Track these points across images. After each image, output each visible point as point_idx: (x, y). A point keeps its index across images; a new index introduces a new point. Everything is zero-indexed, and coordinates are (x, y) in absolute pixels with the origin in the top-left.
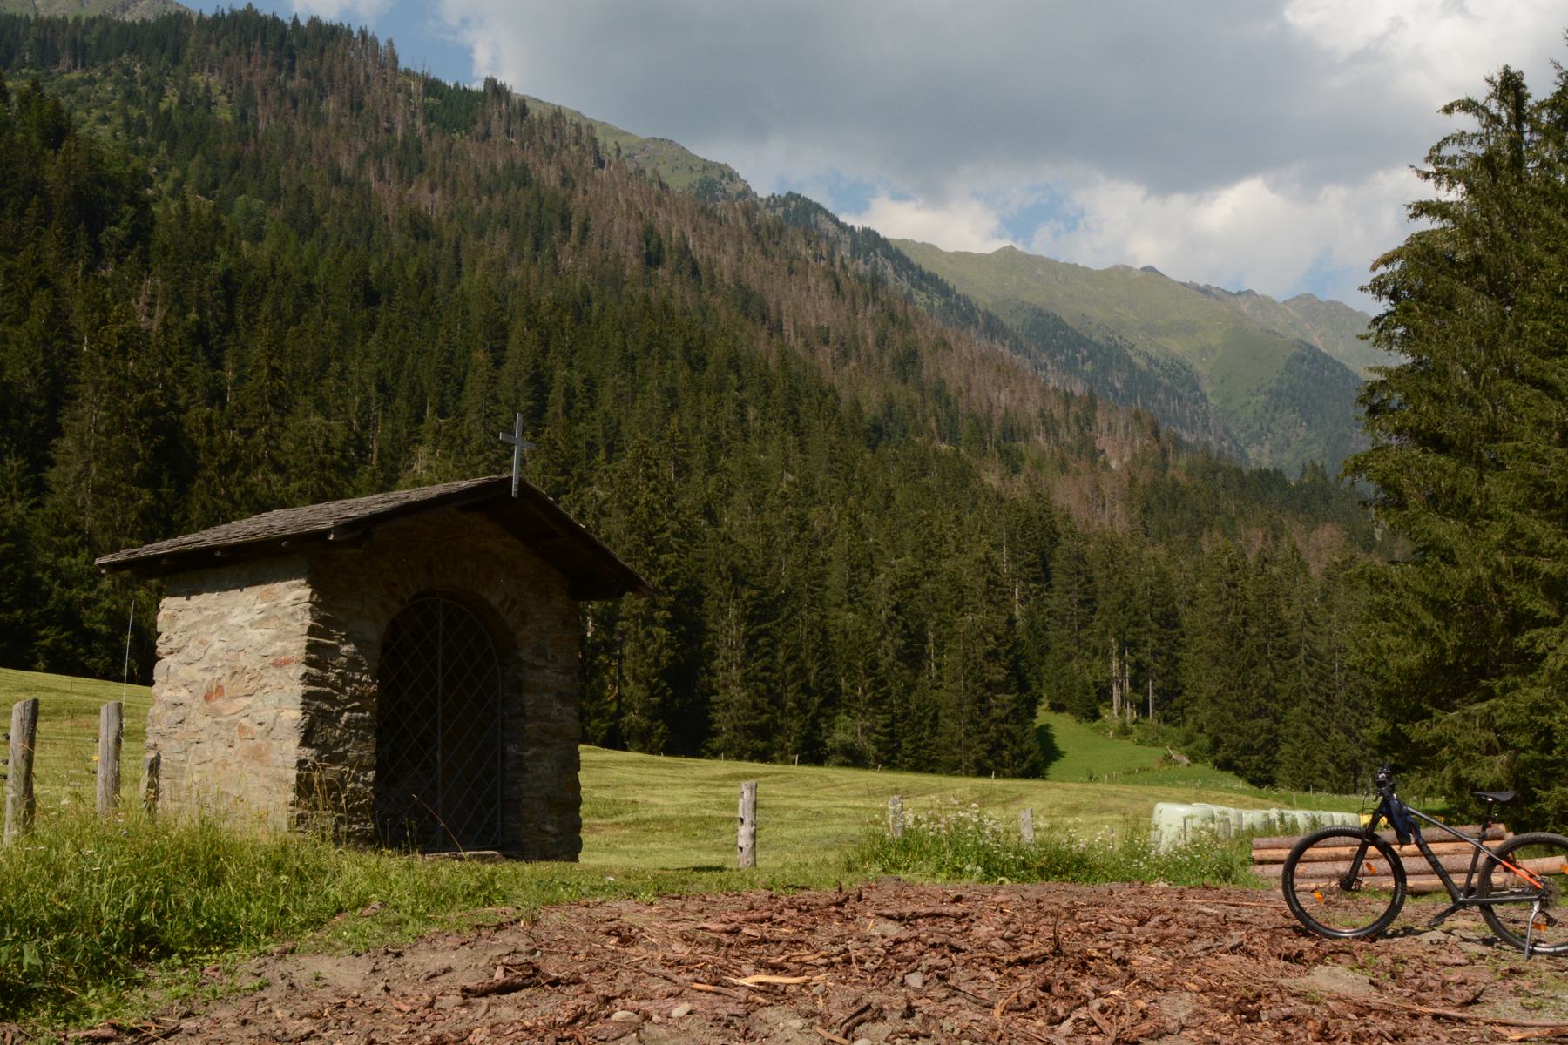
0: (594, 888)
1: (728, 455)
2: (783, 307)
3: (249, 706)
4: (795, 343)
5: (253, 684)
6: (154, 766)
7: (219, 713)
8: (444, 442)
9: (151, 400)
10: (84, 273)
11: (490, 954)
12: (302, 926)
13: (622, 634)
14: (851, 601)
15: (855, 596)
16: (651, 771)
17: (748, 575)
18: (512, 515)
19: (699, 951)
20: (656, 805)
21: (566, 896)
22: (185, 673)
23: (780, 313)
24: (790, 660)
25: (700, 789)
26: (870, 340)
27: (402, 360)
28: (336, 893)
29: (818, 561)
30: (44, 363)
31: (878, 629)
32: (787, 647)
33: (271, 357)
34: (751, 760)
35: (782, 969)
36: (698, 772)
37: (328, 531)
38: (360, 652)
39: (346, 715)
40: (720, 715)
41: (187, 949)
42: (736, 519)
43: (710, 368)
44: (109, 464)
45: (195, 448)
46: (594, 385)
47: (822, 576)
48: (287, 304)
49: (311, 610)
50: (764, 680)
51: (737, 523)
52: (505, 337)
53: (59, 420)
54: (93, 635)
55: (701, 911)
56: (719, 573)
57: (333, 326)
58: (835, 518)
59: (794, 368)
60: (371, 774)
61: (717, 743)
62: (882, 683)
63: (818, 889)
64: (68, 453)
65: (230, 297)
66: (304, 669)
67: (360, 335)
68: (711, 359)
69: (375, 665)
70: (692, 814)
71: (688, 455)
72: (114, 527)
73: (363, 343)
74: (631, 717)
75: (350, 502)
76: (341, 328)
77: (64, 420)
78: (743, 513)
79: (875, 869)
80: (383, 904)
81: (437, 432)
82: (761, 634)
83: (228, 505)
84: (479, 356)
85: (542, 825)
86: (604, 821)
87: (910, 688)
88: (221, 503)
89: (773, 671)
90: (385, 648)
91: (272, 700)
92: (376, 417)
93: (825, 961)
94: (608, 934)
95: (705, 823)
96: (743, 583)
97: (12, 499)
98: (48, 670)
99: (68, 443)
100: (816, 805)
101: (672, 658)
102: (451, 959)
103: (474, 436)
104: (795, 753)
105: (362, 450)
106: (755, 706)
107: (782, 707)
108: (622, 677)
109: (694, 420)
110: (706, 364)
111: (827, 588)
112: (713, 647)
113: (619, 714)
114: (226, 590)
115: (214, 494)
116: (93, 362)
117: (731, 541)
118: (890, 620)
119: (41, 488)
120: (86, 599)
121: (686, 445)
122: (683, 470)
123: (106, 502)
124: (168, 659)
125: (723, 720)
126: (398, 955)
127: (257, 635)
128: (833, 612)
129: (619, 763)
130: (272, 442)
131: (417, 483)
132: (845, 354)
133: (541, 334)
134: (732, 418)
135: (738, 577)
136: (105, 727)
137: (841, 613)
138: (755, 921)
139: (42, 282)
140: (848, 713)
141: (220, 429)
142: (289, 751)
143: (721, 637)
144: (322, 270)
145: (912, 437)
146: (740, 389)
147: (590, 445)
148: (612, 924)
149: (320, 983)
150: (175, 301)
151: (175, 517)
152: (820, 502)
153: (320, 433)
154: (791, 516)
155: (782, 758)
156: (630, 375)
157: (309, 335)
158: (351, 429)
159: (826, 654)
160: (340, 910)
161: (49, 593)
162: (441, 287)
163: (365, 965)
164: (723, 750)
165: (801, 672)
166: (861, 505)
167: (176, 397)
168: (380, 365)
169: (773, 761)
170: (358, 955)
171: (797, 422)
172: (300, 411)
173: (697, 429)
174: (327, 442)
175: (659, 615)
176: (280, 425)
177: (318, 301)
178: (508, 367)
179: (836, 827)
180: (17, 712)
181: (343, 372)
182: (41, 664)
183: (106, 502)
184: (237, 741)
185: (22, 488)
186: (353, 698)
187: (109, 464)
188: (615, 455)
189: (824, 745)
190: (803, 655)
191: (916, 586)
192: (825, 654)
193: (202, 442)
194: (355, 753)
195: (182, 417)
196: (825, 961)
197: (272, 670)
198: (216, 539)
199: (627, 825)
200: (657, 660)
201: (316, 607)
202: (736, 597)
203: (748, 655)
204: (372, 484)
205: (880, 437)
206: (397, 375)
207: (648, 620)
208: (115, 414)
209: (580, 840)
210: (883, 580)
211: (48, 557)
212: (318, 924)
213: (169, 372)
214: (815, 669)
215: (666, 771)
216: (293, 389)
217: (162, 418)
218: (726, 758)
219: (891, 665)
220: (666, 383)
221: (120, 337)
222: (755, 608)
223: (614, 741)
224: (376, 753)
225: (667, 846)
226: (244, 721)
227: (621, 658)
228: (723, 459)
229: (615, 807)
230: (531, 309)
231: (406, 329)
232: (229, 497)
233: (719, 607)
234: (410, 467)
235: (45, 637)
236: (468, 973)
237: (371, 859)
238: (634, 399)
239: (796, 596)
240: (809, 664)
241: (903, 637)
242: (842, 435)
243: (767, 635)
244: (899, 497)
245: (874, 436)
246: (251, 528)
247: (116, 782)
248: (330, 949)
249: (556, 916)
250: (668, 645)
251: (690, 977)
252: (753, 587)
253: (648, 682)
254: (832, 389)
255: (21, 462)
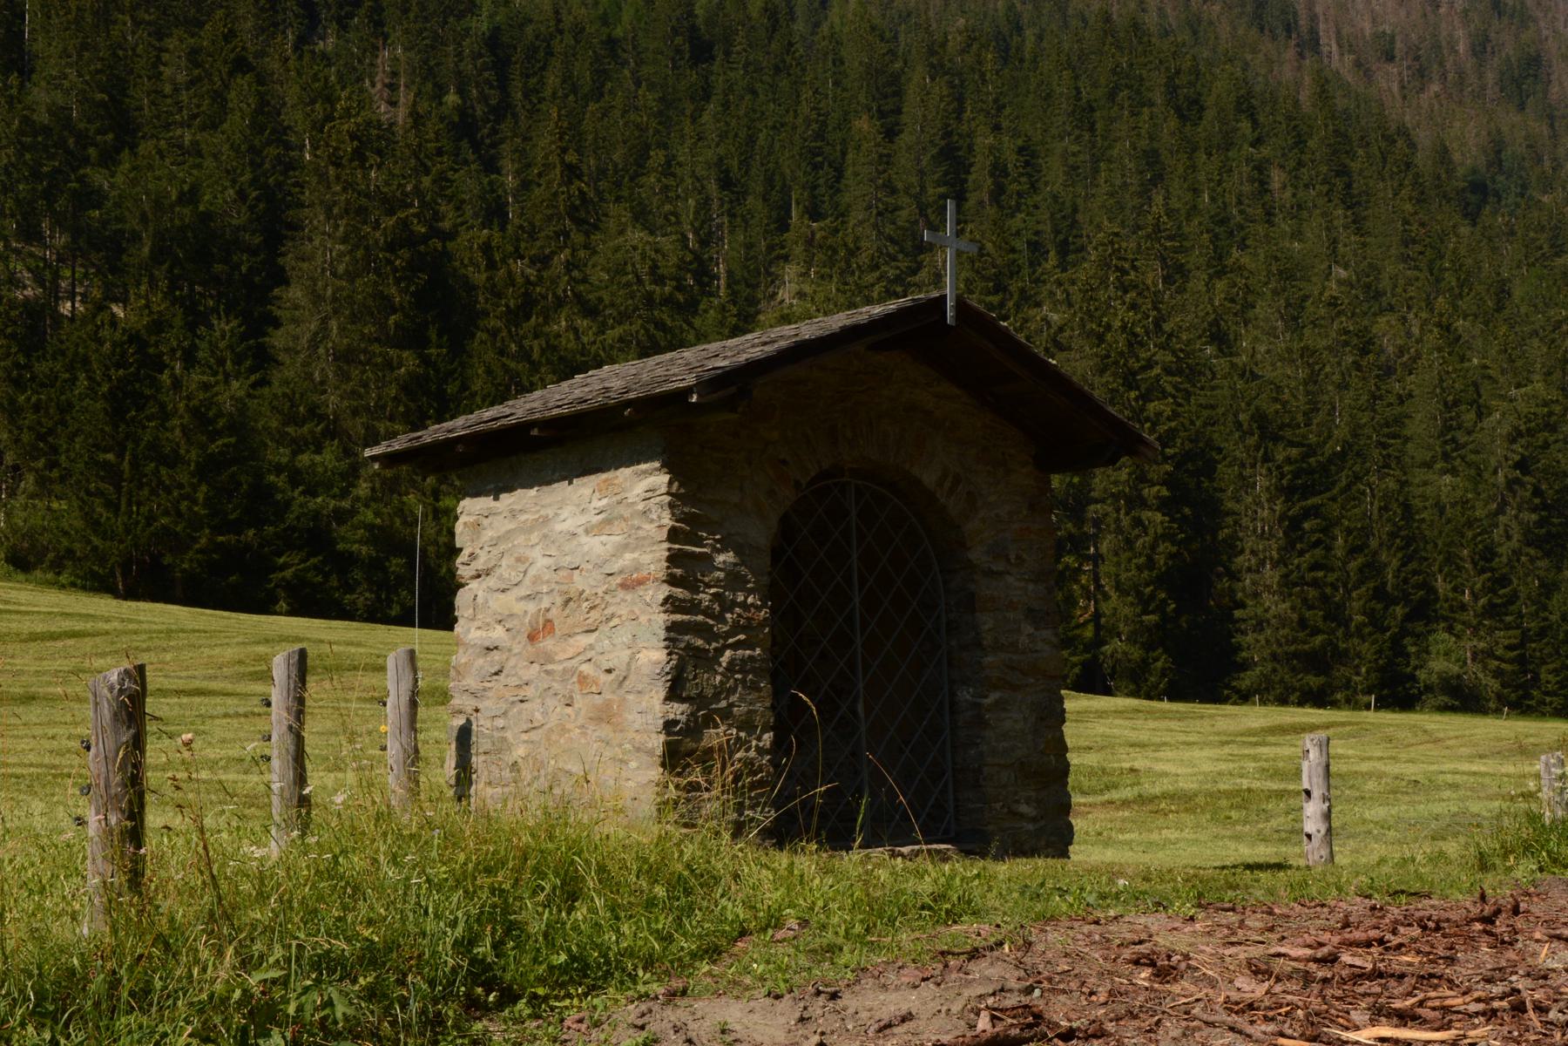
0: (1103, 896)
1: (1243, 246)
2: (1319, 9)
3: (591, 647)
4: (1340, 63)
5: (594, 614)
6: (464, 737)
7: (549, 659)
8: (820, 257)
9: (405, 223)
10: (296, 48)
11: (966, 993)
12: (694, 956)
13: (1097, 523)
14: (1446, 456)
15: (1452, 447)
16: (1152, 724)
17: (1282, 427)
18: (957, 351)
19: (1278, 988)
20: (1165, 774)
21: (1064, 908)
22: (499, 603)
23: (1314, 18)
24: (1353, 551)
25: (1227, 750)
26: (1461, 48)
27: (751, 140)
28: (735, 910)
29: (1392, 399)
30: (254, 181)
31: (1492, 498)
32: (1349, 531)
33: (564, 150)
34: (1301, 704)
35: (1415, 1018)
36: (1222, 724)
37: (688, 391)
38: (743, 563)
39: (728, 653)
40: (1250, 638)
41: (541, 991)
42: (1262, 343)
43: (1210, 114)
44: (354, 319)
45: (471, 288)
46: (1034, 155)
47: (1399, 421)
48: (583, 71)
49: (671, 506)
50: (1315, 583)
51: (1263, 349)
52: (898, 94)
53: (281, 261)
54: (345, 562)
55: (1271, 929)
56: (1239, 425)
57: (650, 98)
58: (1416, 331)
59: (1341, 103)
60: (768, 737)
61: (1247, 680)
62: (1503, 581)
63: (1445, 898)
64: (296, 307)
65: (501, 66)
66: (665, 590)
67: (689, 108)
68: (1209, 101)
69: (765, 580)
70: (1222, 787)
71: (1181, 250)
72: (367, 409)
73: (694, 120)
74: (1115, 646)
75: (714, 346)
76: (662, 100)
77: (288, 261)
78: (1272, 333)
79: (1524, 869)
80: (804, 923)
81: (810, 242)
82: (1307, 513)
83: (521, 367)
84: (863, 124)
85: (1028, 810)
86: (1090, 799)
87: (1548, 589)
88: (513, 365)
89: (1329, 569)
90: (776, 554)
91: (623, 636)
92: (720, 227)
93: (1481, 1006)
94: (1136, 963)
95: (1243, 799)
96: (1276, 439)
97: (227, 376)
98: (292, 612)
99: (296, 293)
100: (1410, 770)
101: (1172, 556)
102: (909, 1001)
103: (864, 244)
104: (1369, 693)
105: (704, 274)
106: (1302, 623)
107: (1346, 623)
108: (1099, 587)
109: (1189, 196)
110: (1202, 109)
111: (1407, 440)
112: (1234, 537)
113: (1099, 642)
114: (549, 483)
115: (502, 353)
116: (323, 177)
117: (1254, 377)
118: (1511, 484)
119: (263, 359)
120: (337, 511)
121: (1177, 235)
122: (1176, 274)
123: (355, 373)
124: (474, 585)
125: (1254, 646)
126: (834, 996)
127: (596, 546)
128: (1419, 476)
129: (1102, 714)
130: (575, 273)
131: (786, 319)
132: (1421, 74)
133: (951, 85)
134: (1247, 188)
135: (1267, 430)
136: (395, 686)
137: (1431, 476)
138: (1357, 944)
139: (241, 65)
140: (1450, 630)
141: (504, 260)
142: (648, 711)
143: (1245, 521)
144: (627, 15)
145: (1537, 195)
146: (1257, 143)
147: (1034, 246)
148: (1142, 949)
149: (729, 1039)
150: (425, 79)
151: (451, 389)
152: (1391, 308)
153: (644, 256)
154: (1346, 332)
155: (1348, 701)
156: (1087, 136)
157: (617, 113)
158: (687, 247)
159: (1409, 541)
160: (743, 933)
161: (288, 504)
162: (799, 26)
163: (787, 1010)
164: (1257, 691)
165: (1373, 568)
166: (1455, 307)
167: (437, 217)
168: (721, 151)
169: (1334, 705)
170: (777, 997)
171: (1349, 186)
172: (612, 225)
173: (1194, 210)
174: (654, 268)
175: (1149, 492)
176: (586, 247)
177: (625, 63)
178: (905, 138)
179: (1445, 805)
180: (280, 666)
181: (668, 163)
182: (283, 605)
183: (355, 373)
184: (577, 697)
185: (238, 361)
186: (736, 628)
187: (354, 319)
188: (1071, 258)
189: (1413, 678)
190: (1374, 543)
191: (1553, 429)
192: (1410, 543)
193: (480, 278)
194: (744, 708)
195: (450, 245)
196: (1481, 1006)
197: (621, 594)
198: (531, 411)
199: (1125, 803)
200: (1150, 559)
201: (677, 501)
202: (1267, 459)
203: (1289, 546)
204: (722, 324)
205: (1484, 201)
206: (745, 163)
207: (1135, 501)
208: (356, 246)
209: (1070, 827)
210: (1498, 422)
211: (282, 455)
212: (713, 952)
213: (426, 181)
214: (1395, 563)
215: (1174, 725)
216: (599, 193)
217: (422, 248)
218: (1263, 703)
219: (1517, 553)
220: (1143, 143)
221: (353, 137)
222: (1296, 475)
223: (1094, 682)
224: (773, 707)
225: (1187, 834)
226: (586, 668)
227: (1097, 559)
228: (1235, 253)
229: (1107, 780)
230: (934, 49)
231: (754, 93)
232: (525, 355)
233: (1241, 477)
234: (775, 294)
235: (283, 568)
236: (941, 1021)
237: (782, 859)
238: (1096, 171)
239: (1358, 454)
240: (1384, 557)
241: (1534, 510)
242: (1421, 200)
243: (1316, 516)
244: (1518, 293)
245: (1473, 198)
246: (578, 393)
247: (414, 756)
248: (735, 989)
249: (1055, 937)
250: (1167, 536)
251: (1271, 1028)
252: (1291, 444)
253: (1139, 594)
254: (1403, 132)
255: (234, 323)
